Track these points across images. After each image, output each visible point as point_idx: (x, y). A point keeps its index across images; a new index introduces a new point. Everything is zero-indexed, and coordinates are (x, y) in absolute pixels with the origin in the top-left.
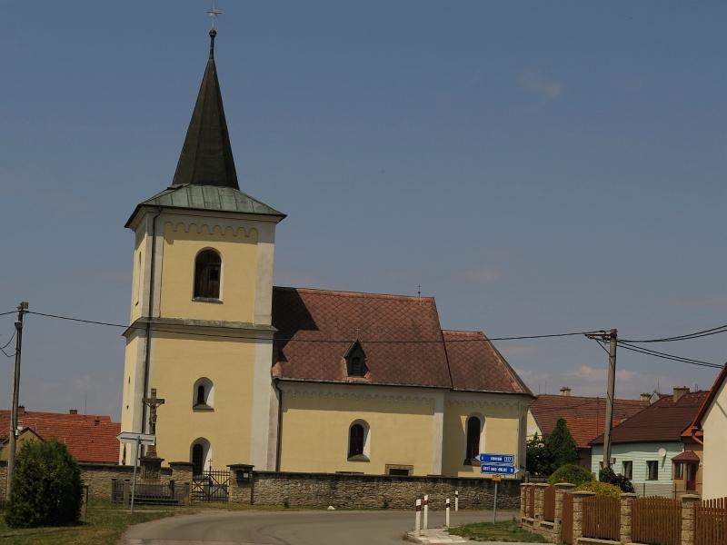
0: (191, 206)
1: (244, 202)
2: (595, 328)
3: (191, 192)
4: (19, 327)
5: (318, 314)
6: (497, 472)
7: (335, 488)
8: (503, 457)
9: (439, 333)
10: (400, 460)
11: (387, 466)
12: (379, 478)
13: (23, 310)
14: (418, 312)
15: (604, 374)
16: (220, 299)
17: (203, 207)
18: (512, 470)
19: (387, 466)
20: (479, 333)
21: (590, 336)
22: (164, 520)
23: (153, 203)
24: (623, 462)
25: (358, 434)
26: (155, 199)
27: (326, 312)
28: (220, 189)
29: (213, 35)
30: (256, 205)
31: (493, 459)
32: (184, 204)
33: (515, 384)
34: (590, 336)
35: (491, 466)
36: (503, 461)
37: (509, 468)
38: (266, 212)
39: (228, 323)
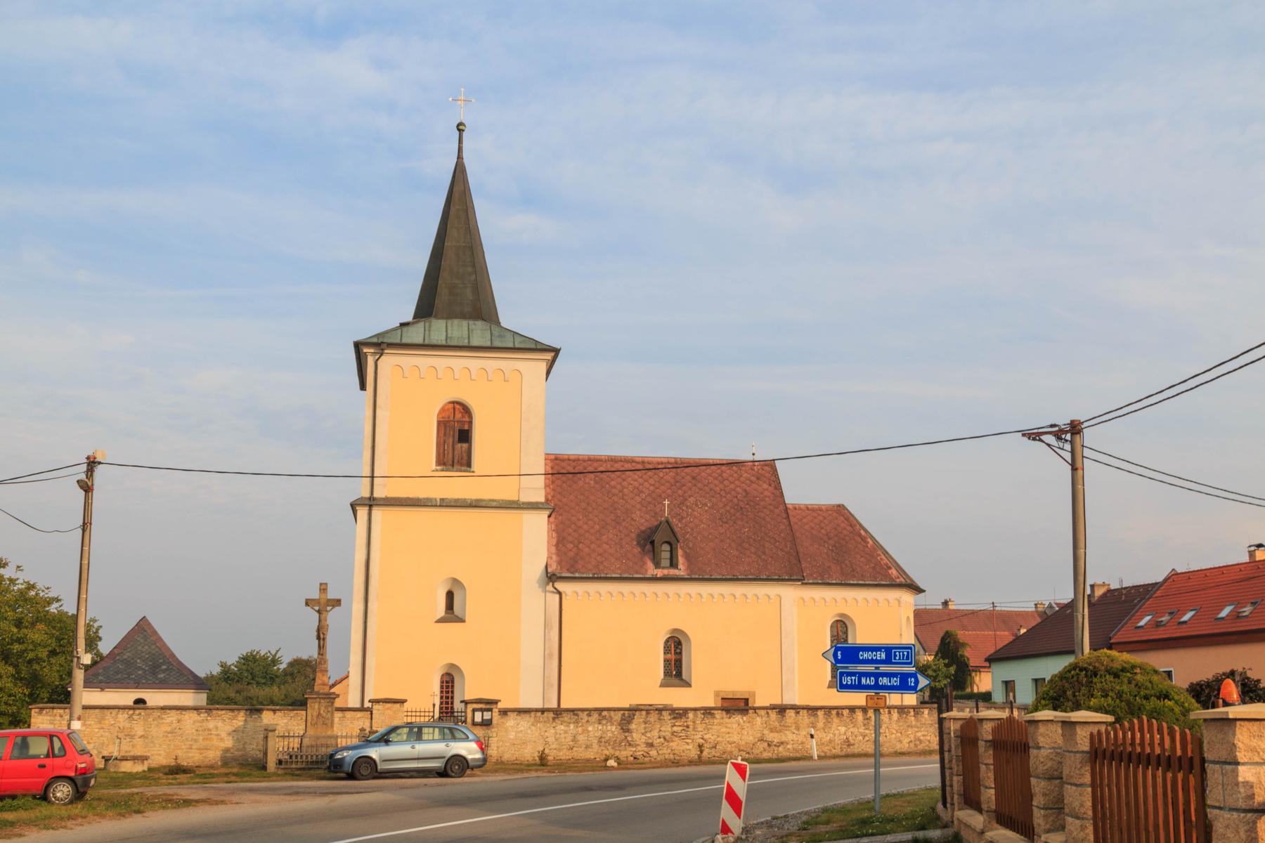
0: (426, 342)
1: (501, 336)
2: (1031, 424)
3: (430, 326)
4: (87, 488)
5: (615, 487)
6: (877, 676)
7: (628, 731)
8: (889, 650)
9: (782, 507)
10: (736, 686)
11: (717, 694)
12: (708, 712)
13: (92, 464)
14: (754, 479)
15: (871, 734)
16: (472, 470)
17: (444, 343)
18: (911, 681)
19: (717, 694)
20: (839, 506)
21: (1034, 436)
22: (1080, 712)
23: (375, 340)
24: (1033, 679)
25: (676, 646)
26: (378, 335)
27: (625, 484)
28: (471, 322)
29: (460, 128)
30: (518, 339)
31: (866, 655)
32: (419, 340)
33: (893, 572)
34: (1034, 436)
35: (862, 675)
36: (888, 661)
37: (904, 677)
38: (533, 346)
39: (484, 500)
